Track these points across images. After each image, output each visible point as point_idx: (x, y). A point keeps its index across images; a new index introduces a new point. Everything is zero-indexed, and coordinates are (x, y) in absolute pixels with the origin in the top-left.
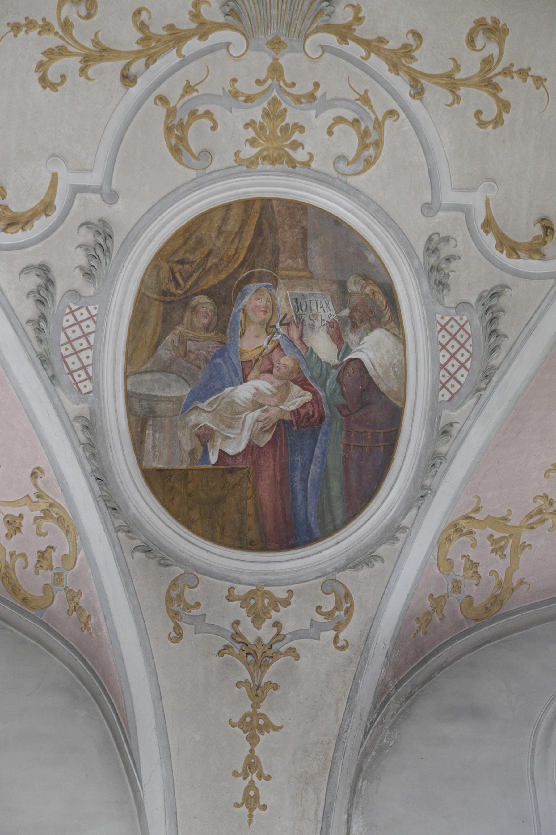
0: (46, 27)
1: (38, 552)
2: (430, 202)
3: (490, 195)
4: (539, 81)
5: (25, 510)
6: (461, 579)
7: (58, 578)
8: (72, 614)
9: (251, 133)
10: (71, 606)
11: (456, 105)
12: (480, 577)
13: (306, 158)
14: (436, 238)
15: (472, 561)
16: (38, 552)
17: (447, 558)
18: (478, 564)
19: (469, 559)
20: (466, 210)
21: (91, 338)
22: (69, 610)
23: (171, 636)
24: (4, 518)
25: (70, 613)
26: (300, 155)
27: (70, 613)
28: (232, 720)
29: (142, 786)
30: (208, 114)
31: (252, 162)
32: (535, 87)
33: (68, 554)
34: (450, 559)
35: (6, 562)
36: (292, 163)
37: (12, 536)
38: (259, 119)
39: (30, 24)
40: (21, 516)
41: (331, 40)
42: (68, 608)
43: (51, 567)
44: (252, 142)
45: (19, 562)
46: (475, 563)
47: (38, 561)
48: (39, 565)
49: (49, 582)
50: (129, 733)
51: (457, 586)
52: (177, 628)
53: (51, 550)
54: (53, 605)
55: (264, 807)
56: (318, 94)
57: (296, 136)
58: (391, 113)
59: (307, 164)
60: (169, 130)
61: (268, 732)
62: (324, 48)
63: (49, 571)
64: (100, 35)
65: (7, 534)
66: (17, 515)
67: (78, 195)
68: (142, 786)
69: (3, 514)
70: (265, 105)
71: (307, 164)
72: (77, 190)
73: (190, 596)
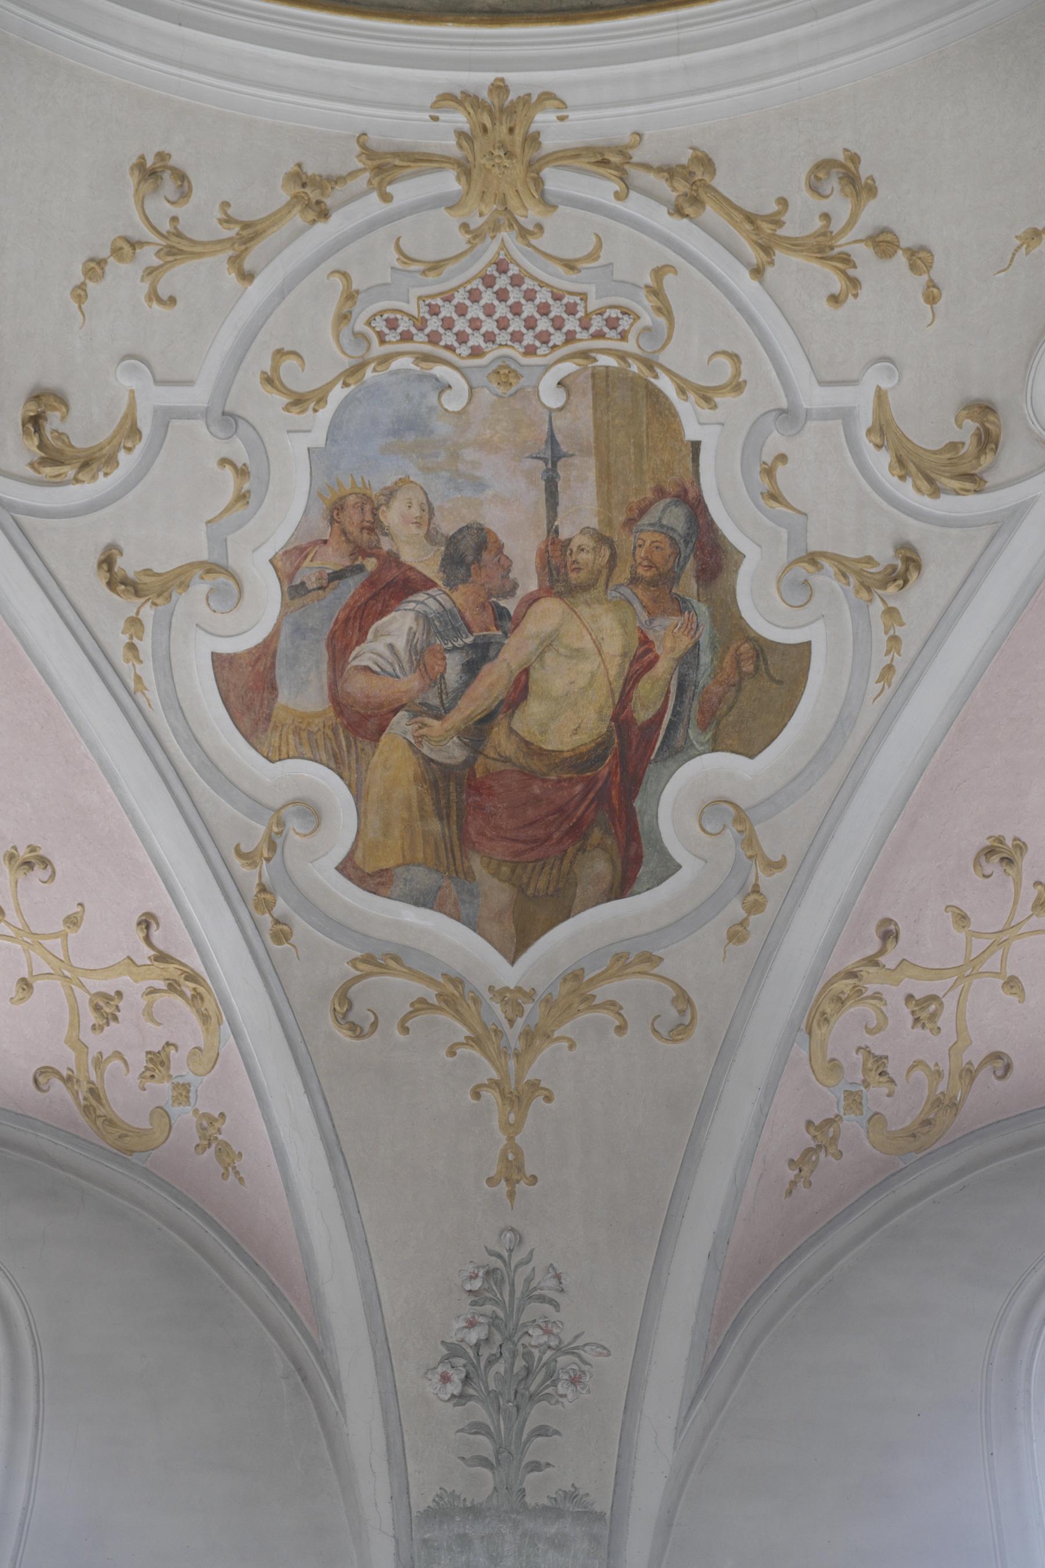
12: (892, 1081)
20: (846, 416)
69: (88, 992)
72: (166, 417)
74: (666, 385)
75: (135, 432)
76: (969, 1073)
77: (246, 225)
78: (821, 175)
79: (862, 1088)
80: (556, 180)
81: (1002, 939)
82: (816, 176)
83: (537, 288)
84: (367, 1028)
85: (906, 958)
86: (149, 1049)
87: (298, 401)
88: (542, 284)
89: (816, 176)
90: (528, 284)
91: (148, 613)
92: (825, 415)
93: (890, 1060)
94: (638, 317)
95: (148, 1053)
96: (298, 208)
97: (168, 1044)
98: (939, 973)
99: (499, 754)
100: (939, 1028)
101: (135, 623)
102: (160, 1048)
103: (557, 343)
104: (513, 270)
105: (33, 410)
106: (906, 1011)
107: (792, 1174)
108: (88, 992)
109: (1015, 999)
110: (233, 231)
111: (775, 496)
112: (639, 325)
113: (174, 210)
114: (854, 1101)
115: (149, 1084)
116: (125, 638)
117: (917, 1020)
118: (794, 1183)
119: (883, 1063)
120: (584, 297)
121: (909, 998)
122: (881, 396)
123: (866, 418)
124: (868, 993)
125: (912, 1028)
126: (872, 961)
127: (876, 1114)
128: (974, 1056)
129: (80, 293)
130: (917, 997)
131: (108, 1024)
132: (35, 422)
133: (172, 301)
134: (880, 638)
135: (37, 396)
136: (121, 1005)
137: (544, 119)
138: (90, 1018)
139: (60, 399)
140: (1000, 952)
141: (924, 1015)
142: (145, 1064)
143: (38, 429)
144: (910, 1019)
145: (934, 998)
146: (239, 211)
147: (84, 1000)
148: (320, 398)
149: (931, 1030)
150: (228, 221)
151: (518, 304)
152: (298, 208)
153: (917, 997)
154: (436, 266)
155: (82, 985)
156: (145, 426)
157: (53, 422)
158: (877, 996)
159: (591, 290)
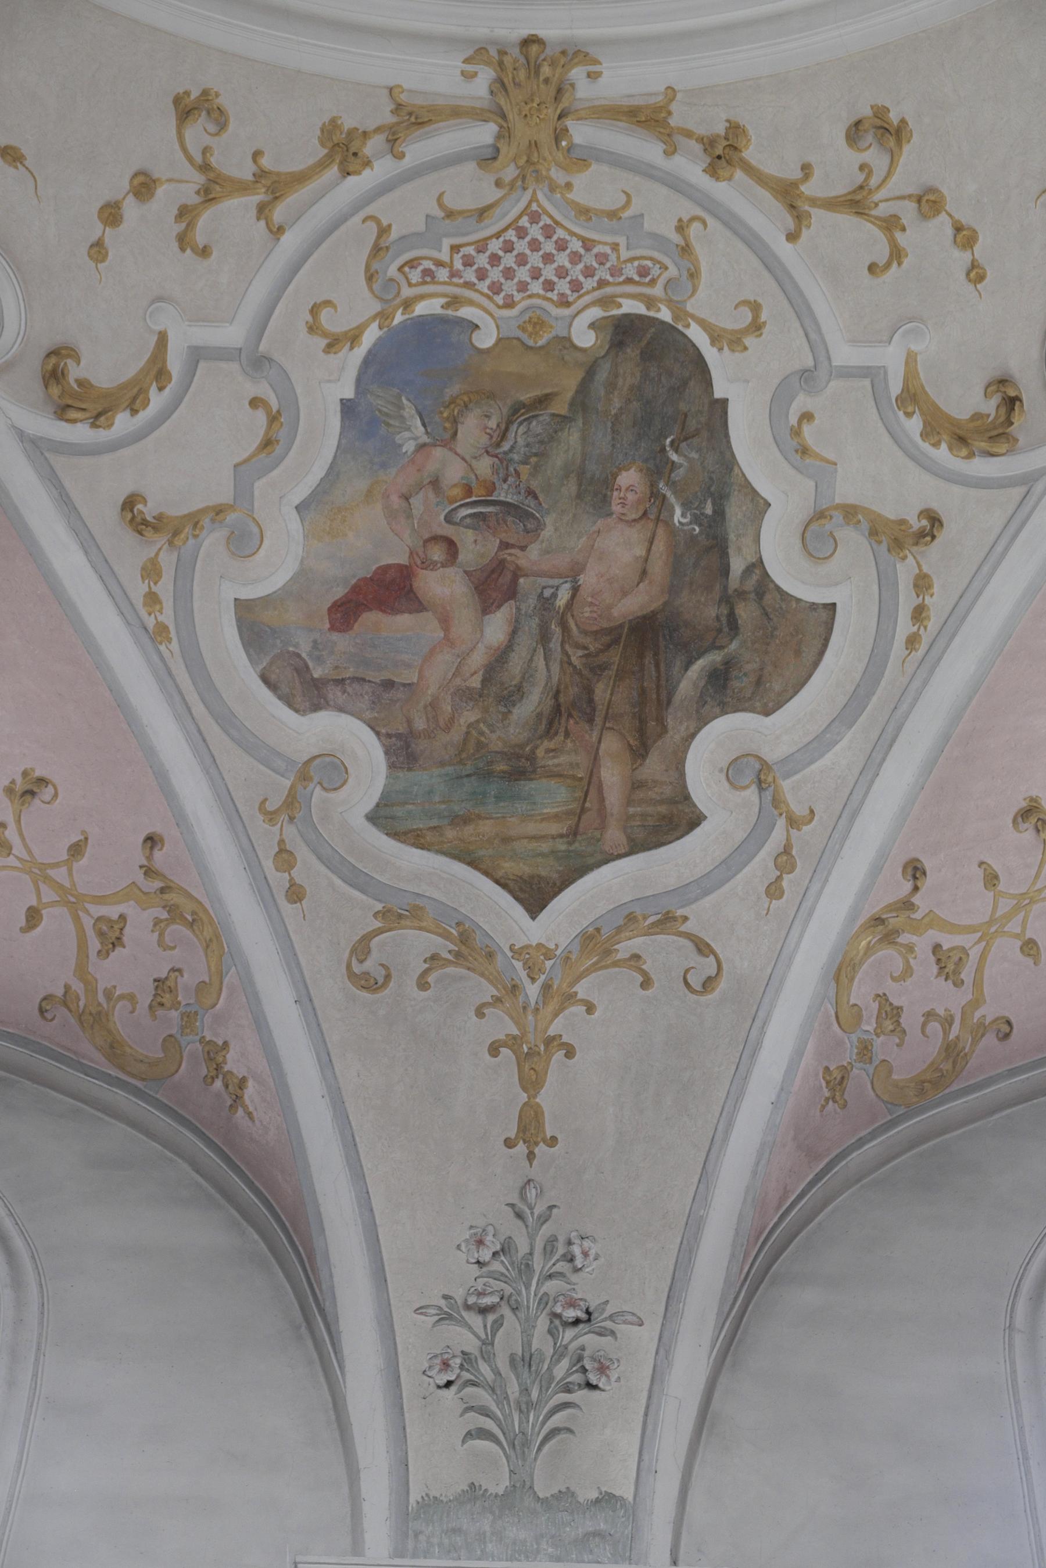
1: (155, 980)
2: (810, 363)
3: (914, 347)
5: (128, 908)
10: (211, 1069)
14: (602, 1353)
16: (155, 980)
17: (851, 1003)
19: (887, 1000)
20: (873, 375)
22: (206, 1076)
24: (94, 925)
33: (207, 980)
35: (99, 1004)
37: (108, 954)
40: (122, 917)
43: (176, 1005)
45: (120, 1009)
47: (155, 995)
48: (156, 1005)
49: (174, 1031)
50: (321, 1290)
51: (865, 1050)
53: (177, 973)
55: (807, 169)
63: (173, 1011)
65: (99, 952)
66: (115, 917)
67: (202, 365)
69: (92, 917)
72: (197, 355)
74: (697, 335)
75: (161, 375)
76: (980, 1030)
79: (875, 1037)
80: (580, 133)
81: (1025, 902)
83: (568, 238)
84: (381, 981)
86: (155, 976)
87: (333, 344)
88: (572, 234)
90: (560, 233)
91: (167, 561)
92: (848, 373)
94: (666, 268)
96: (805, 420)
101: (151, 571)
103: (494, 240)
104: (545, 220)
108: (92, 917)
109: (1030, 961)
111: (804, 451)
112: (666, 275)
113: (208, 140)
114: (865, 1050)
116: (143, 588)
120: (615, 247)
122: (911, 359)
127: (884, 1061)
128: (988, 1012)
129: (98, 250)
133: (204, 252)
134: (906, 601)
137: (577, 74)
138: (94, 944)
140: (1023, 913)
147: (88, 923)
148: (353, 338)
151: (573, 263)
152: (805, 420)
154: (482, 213)
155: (87, 912)
156: (175, 364)
159: (622, 241)
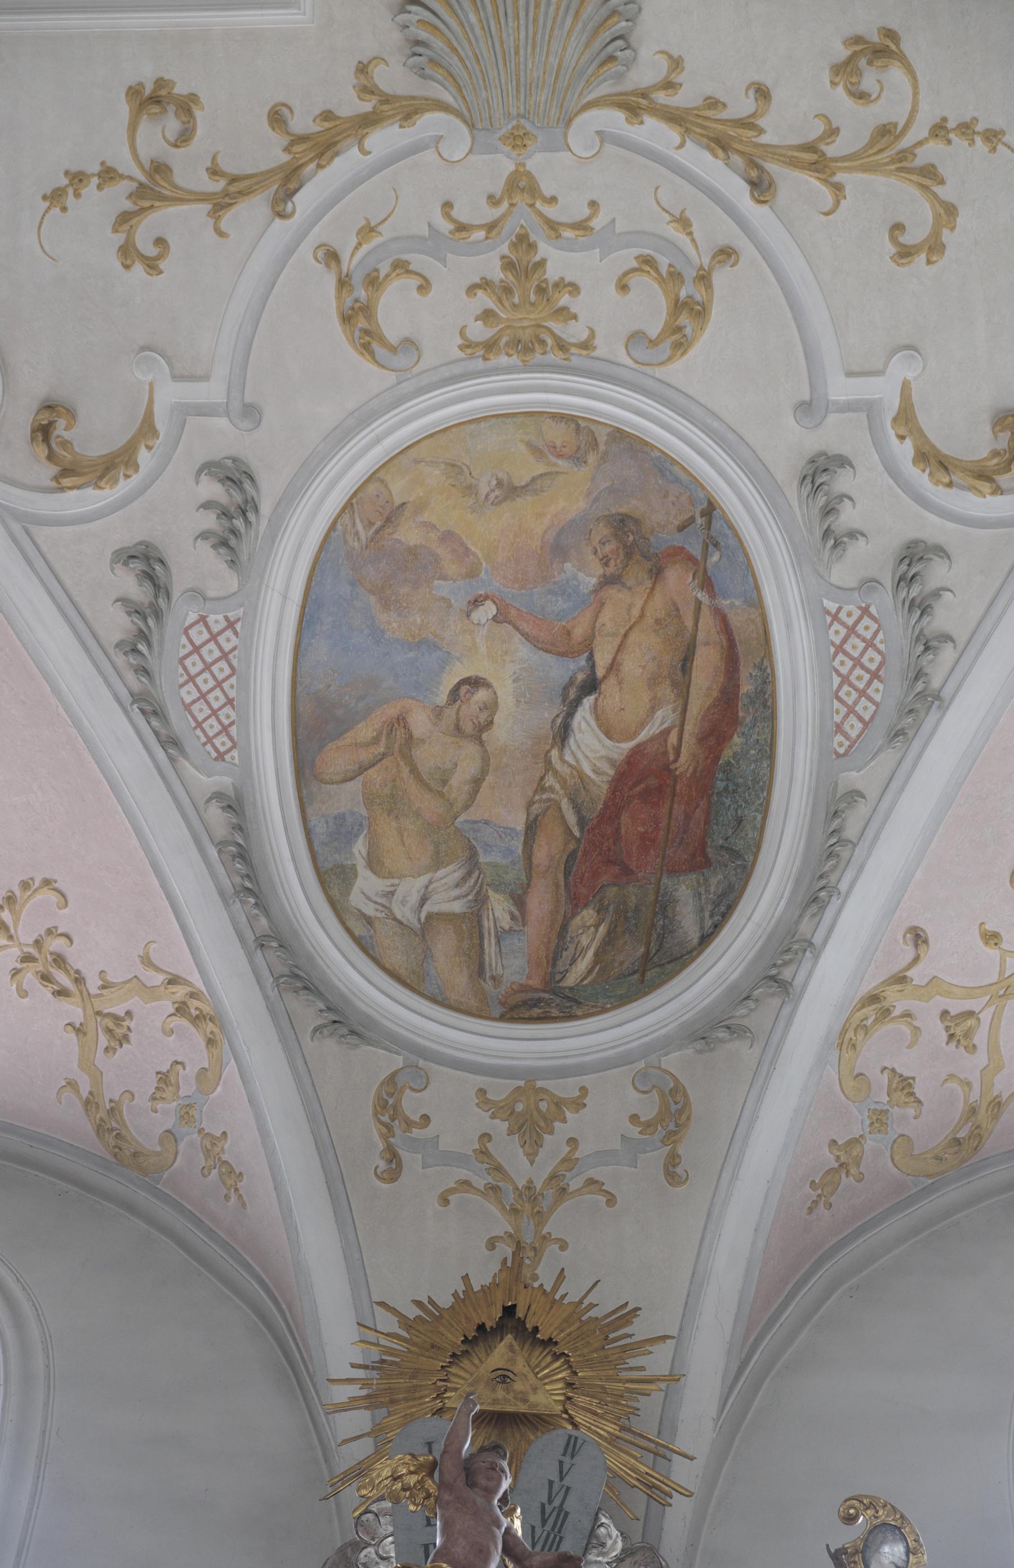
0: (108, 175)
4: (993, 136)
6: (887, 1107)
7: (186, 1114)
8: (210, 1174)
9: (484, 300)
11: (843, 202)
12: (919, 1102)
13: (584, 335)
15: (901, 1076)
18: (913, 1078)
20: (869, 408)
21: (233, 730)
22: (204, 1168)
23: (379, 1171)
25: (206, 1171)
26: (574, 332)
27: (206, 1171)
28: (382, 66)
29: (314, 1385)
30: (401, 267)
31: (490, 346)
32: (919, 472)
34: (861, 1074)
36: (562, 346)
38: (497, 274)
39: (78, 178)
41: (614, 119)
42: (203, 1164)
44: (487, 316)
46: (907, 1079)
52: (392, 1156)
54: (176, 1164)
56: (597, 223)
57: (565, 300)
58: (726, 254)
59: (586, 345)
60: (346, 319)
61: (564, 1120)
62: (602, 135)
64: (219, 159)
68: (314, 1385)
70: (505, 249)
71: (586, 345)
72: (186, 411)
73: (411, 1104)
77: (234, 180)
78: (854, 80)
82: (850, 83)
85: (937, 975)
89: (850, 83)
92: (850, 407)
93: (917, 1080)
95: (158, 1073)
97: (177, 1062)
98: (970, 992)
99: (635, 972)
100: (974, 1046)
102: (169, 1068)
105: (44, 419)
106: (940, 1026)
107: (813, 1195)
110: (218, 185)
114: (879, 1119)
115: (160, 1106)
117: (951, 1036)
118: (815, 1203)
119: (910, 1083)
121: (945, 1013)
123: (893, 404)
124: (897, 1012)
125: (947, 1044)
126: (900, 979)
130: (953, 1013)
131: (121, 1045)
132: (43, 432)
135: (49, 407)
136: (132, 1025)
139: (71, 414)
141: (959, 1031)
142: (156, 1085)
143: (46, 439)
144: (944, 1036)
145: (971, 1014)
146: (229, 166)
149: (965, 1047)
150: (214, 172)
153: (953, 1013)
157: (60, 430)
158: (907, 1015)
